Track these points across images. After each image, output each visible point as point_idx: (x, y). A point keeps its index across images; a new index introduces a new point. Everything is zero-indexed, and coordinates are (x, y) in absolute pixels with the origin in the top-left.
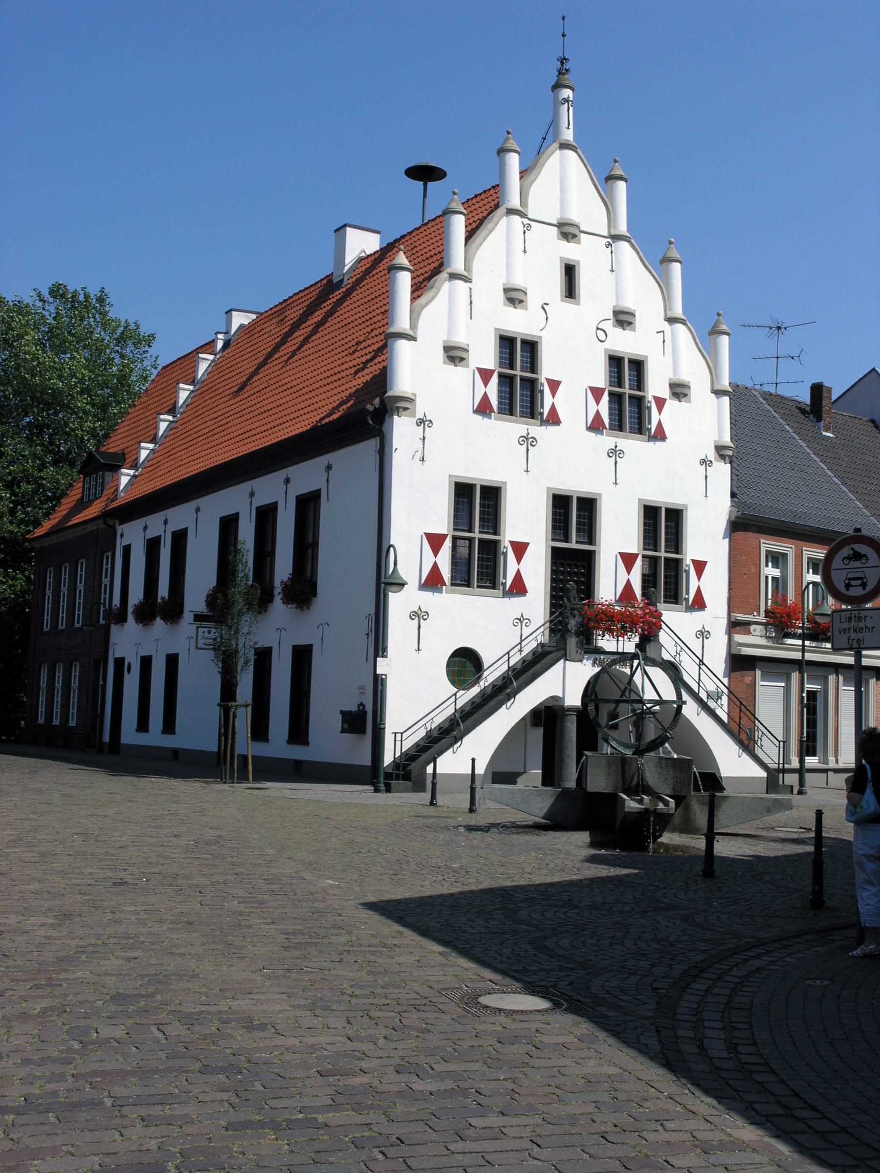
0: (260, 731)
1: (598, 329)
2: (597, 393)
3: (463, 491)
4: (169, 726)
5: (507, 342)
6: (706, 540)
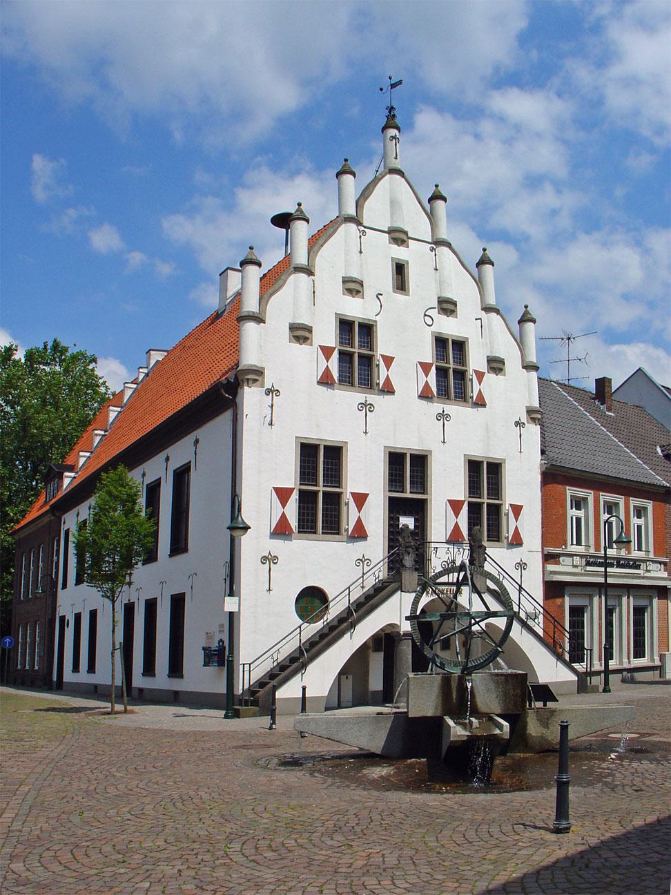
0: (149, 669)
1: (425, 315)
2: (425, 367)
3: (308, 451)
4: (92, 668)
5: (345, 326)
6: (522, 487)
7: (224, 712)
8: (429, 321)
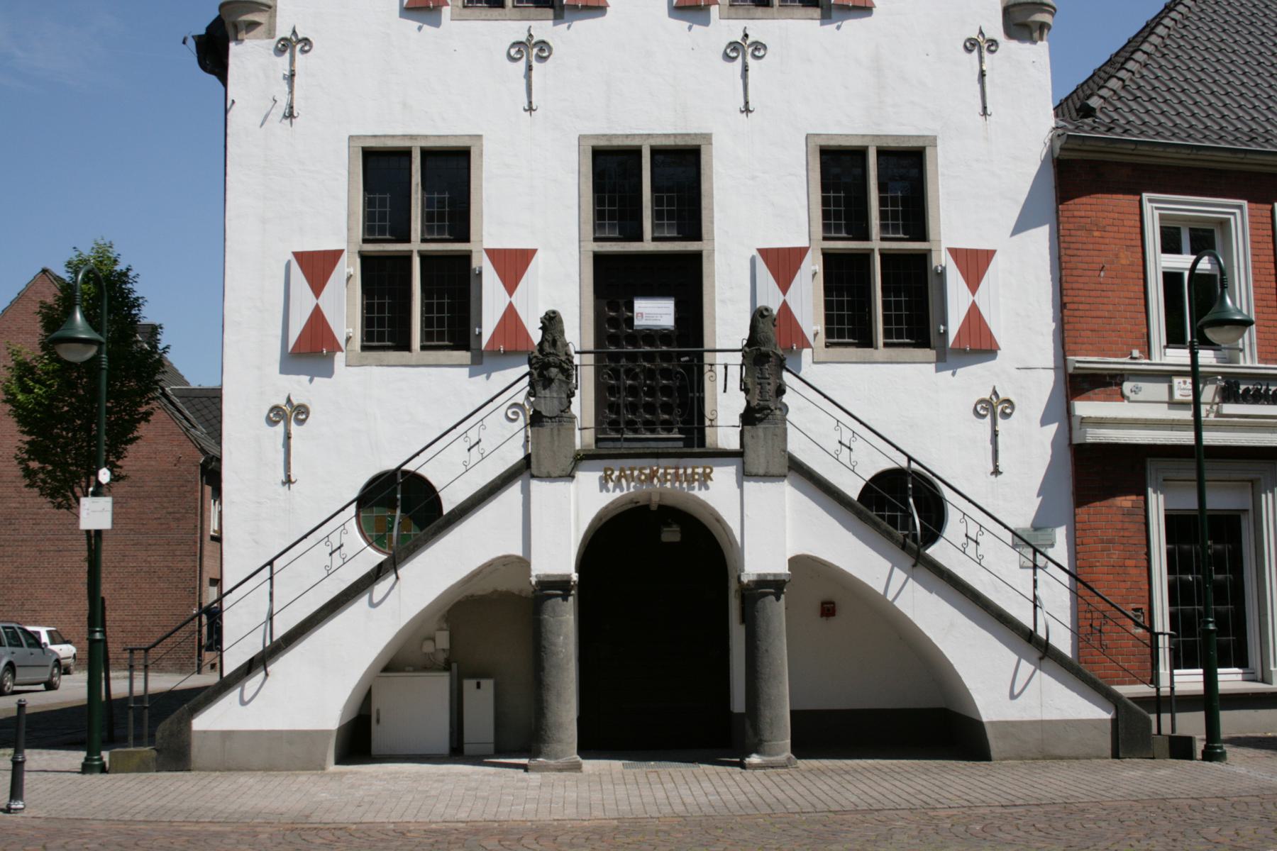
3: (382, 167)
7: (83, 754)
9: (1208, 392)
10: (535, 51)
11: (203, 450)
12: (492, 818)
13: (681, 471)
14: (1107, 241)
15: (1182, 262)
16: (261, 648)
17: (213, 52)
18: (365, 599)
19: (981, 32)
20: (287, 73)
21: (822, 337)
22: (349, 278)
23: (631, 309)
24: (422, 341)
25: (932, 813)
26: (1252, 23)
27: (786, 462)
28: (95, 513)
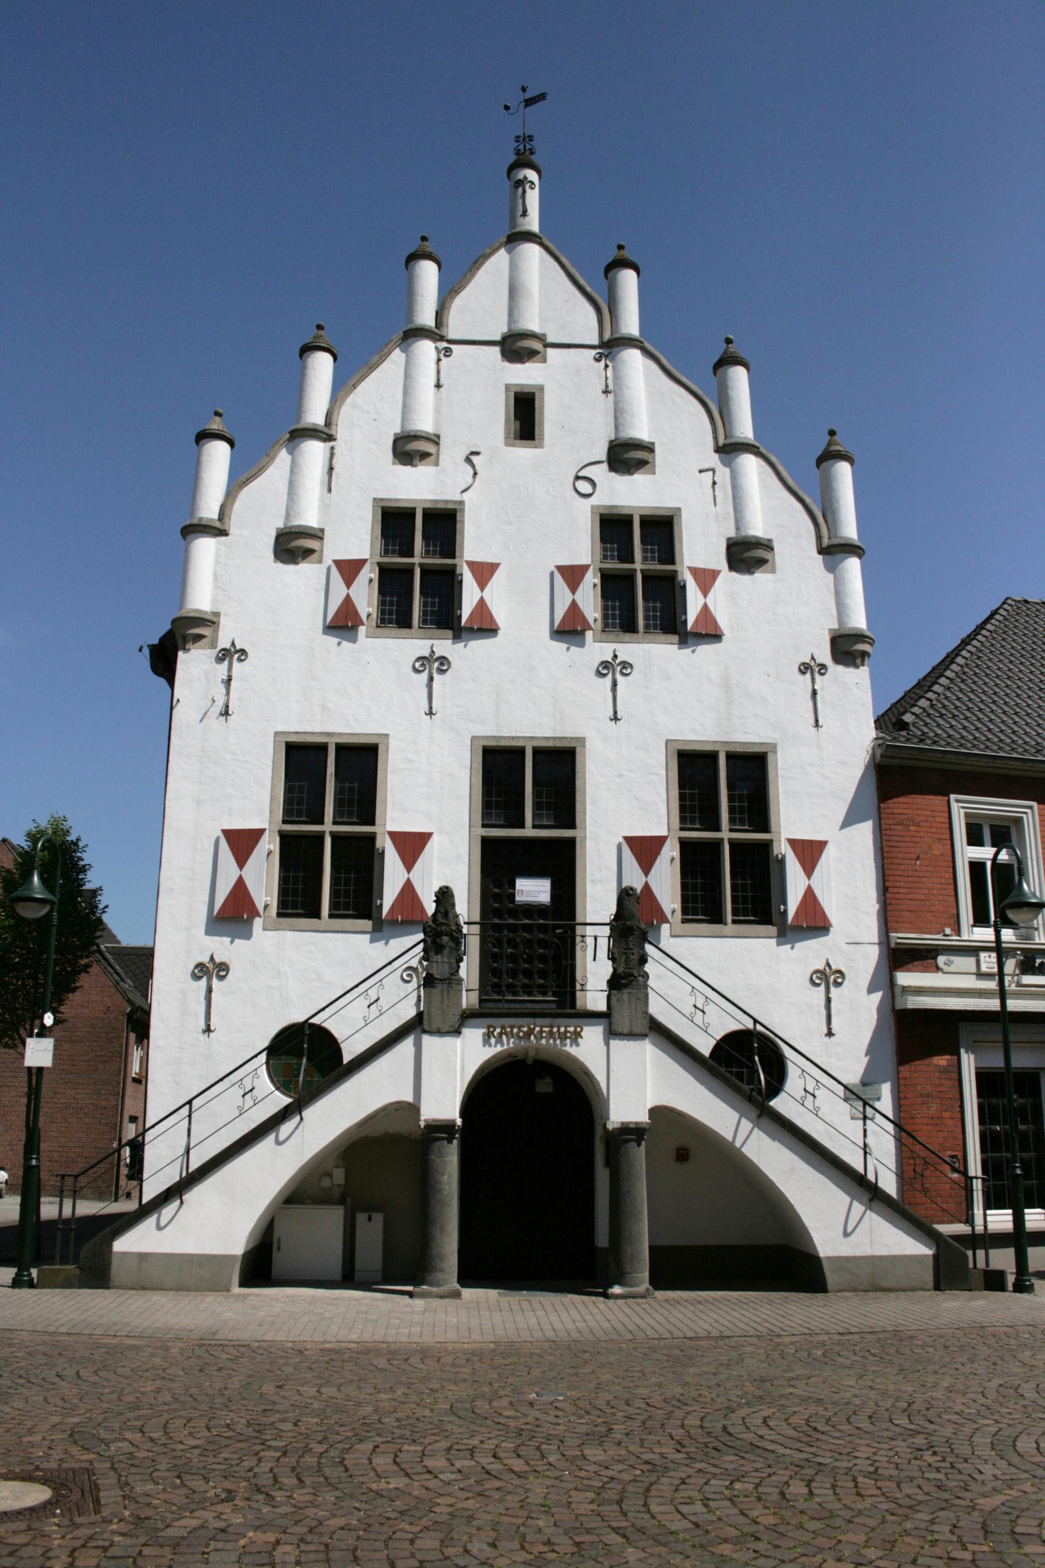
3: (302, 759)
5: (395, 522)
7: (15, 1270)
8: (584, 487)
9: (1010, 965)
10: (436, 664)
11: (130, 1002)
12: (381, 1339)
13: (555, 1030)
14: (922, 834)
15: (985, 853)
16: (177, 1179)
17: (164, 660)
18: (271, 1138)
19: (813, 658)
20: (225, 678)
21: (599, 625)
22: (270, 853)
23: (513, 887)
24: (330, 910)
25: (777, 1340)
26: (1033, 657)
27: (646, 1022)
28: (39, 1053)
